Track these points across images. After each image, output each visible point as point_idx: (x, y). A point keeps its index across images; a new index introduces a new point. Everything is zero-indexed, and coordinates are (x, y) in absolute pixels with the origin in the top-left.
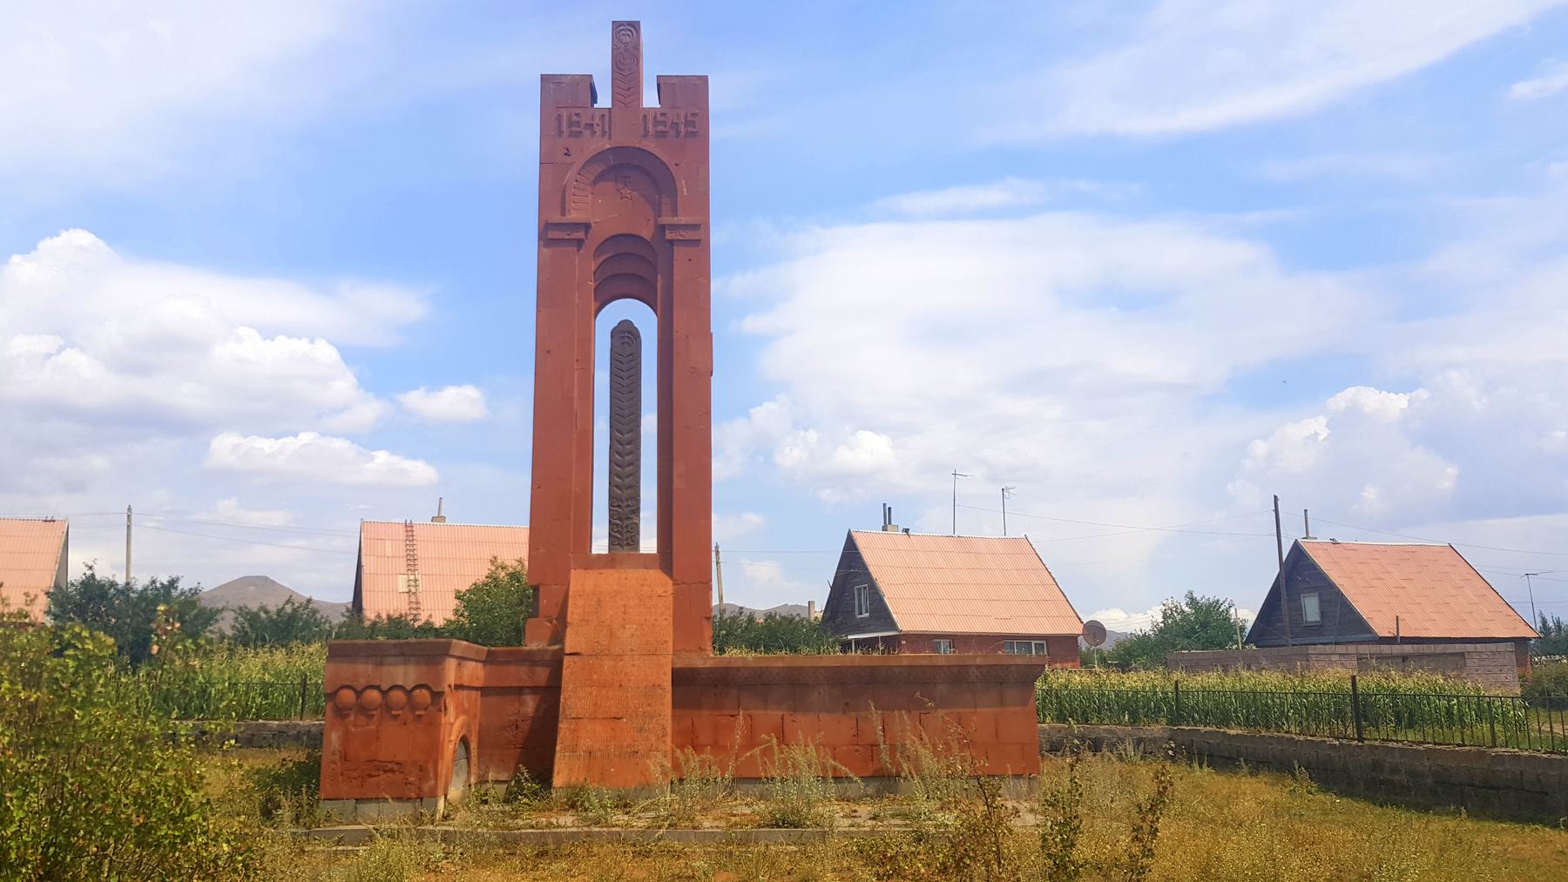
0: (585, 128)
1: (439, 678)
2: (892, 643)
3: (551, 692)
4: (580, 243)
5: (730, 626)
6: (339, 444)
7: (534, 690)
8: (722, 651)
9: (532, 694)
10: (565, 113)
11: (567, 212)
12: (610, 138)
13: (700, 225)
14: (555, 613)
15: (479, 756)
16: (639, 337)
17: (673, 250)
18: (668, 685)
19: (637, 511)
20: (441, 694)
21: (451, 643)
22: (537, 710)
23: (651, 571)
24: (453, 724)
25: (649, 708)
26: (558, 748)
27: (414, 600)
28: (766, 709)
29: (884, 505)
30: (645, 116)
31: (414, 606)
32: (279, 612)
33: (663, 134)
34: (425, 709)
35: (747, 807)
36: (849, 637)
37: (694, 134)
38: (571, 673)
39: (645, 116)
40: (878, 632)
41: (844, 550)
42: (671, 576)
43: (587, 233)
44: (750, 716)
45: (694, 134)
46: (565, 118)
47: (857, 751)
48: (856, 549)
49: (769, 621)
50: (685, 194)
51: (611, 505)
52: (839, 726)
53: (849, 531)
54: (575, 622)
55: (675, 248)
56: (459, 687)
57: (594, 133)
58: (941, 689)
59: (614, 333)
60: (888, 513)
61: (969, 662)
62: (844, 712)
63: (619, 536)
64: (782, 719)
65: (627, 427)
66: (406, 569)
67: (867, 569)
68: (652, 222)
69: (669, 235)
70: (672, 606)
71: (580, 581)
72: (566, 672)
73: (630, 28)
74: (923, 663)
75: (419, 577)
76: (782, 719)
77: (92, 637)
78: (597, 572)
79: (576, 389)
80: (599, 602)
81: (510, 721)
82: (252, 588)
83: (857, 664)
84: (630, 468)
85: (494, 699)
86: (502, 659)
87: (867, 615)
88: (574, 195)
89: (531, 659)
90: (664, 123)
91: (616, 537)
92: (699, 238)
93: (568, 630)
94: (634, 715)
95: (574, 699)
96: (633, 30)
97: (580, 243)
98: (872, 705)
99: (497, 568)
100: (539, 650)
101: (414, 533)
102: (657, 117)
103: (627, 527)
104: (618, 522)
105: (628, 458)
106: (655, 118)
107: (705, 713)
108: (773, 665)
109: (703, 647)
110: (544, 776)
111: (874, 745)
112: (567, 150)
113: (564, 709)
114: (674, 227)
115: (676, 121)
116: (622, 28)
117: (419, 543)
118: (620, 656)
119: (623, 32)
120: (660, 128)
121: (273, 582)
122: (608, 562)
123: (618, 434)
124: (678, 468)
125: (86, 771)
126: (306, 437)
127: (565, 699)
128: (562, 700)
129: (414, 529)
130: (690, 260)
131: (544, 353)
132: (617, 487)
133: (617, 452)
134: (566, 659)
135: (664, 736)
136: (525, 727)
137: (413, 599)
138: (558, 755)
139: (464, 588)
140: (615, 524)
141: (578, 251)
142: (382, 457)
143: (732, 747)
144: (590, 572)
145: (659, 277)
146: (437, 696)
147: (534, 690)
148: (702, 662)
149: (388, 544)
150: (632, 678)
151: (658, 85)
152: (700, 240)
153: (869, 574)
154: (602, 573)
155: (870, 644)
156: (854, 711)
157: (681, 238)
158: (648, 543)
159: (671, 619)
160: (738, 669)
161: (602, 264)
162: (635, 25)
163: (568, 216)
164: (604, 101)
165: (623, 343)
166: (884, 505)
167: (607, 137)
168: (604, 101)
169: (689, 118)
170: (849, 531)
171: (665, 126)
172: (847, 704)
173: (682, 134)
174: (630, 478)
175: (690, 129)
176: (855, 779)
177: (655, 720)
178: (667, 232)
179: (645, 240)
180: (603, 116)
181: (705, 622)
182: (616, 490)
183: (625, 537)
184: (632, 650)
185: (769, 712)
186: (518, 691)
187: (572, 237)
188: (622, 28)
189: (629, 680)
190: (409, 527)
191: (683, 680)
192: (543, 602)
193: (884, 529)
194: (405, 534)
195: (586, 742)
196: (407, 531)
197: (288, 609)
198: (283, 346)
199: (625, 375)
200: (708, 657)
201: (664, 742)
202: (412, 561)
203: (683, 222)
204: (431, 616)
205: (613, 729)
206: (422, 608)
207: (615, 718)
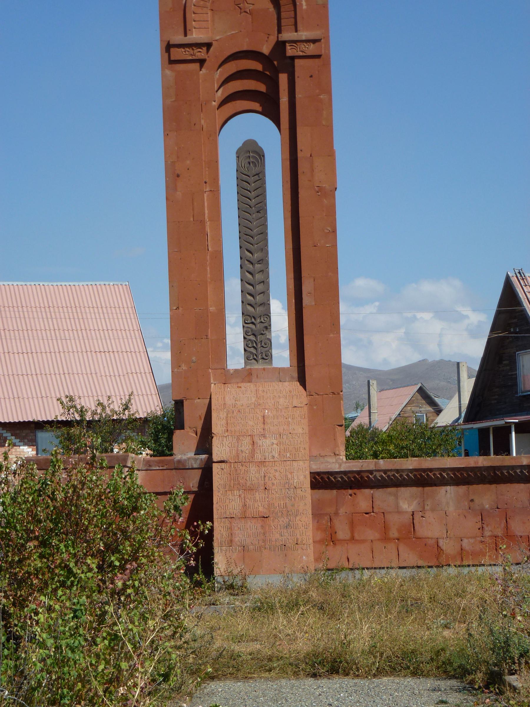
4: (202, 62)
13: (321, 39)
14: (199, 425)
16: (264, 156)
19: (268, 328)
23: (286, 384)
42: (305, 390)
59: (239, 153)
69: (290, 51)
70: (306, 416)
79: (206, 212)
86: (158, 468)
88: (194, 13)
91: (251, 353)
109: (337, 453)
124: (307, 287)
125: (106, 528)
130: (311, 76)
133: (248, 272)
134: (215, 466)
150: (275, 482)
154: (240, 387)
165: (249, 163)
207: (264, 517)
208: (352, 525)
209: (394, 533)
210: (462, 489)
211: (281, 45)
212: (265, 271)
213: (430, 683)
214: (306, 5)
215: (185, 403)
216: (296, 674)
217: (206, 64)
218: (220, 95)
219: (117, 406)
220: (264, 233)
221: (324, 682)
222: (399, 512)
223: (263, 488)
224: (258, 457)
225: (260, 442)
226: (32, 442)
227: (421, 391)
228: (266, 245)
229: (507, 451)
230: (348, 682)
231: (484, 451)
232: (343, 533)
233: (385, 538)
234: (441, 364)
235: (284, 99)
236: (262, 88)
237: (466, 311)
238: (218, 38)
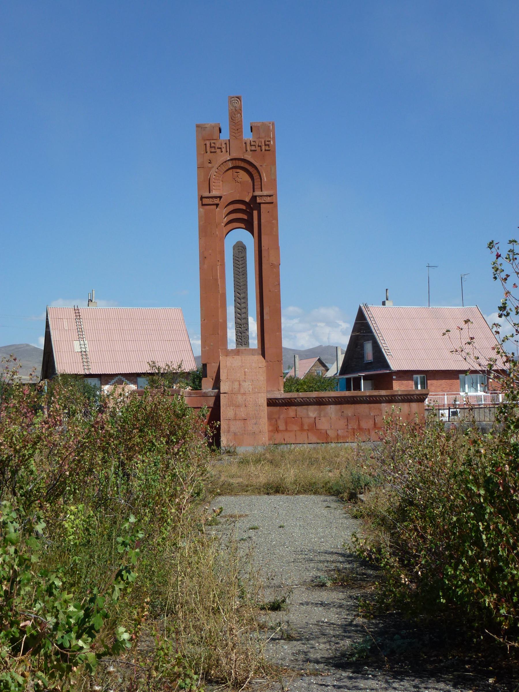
19: (247, 330)
30: (245, 143)
41: (356, 320)
46: (208, 145)
59: (234, 247)
63: (241, 341)
64: (315, 419)
67: (371, 332)
69: (259, 200)
73: (236, 99)
76: (315, 419)
96: (238, 100)
97: (217, 205)
101: (81, 317)
109: (280, 389)
110: (218, 444)
115: (260, 144)
116: (233, 99)
117: (84, 320)
119: (233, 101)
122: (237, 352)
129: (80, 311)
131: (203, 258)
148: (279, 395)
151: (251, 127)
157: (264, 202)
158: (254, 343)
168: (225, 136)
179: (245, 201)
189: (249, 404)
191: (272, 403)
194: (75, 315)
196: (79, 313)
208: (286, 423)
209: (306, 427)
210: (338, 407)
211: (254, 198)
212: (246, 303)
213: (322, 498)
214: (267, 179)
215: (207, 365)
216: (259, 493)
217: (219, 206)
218: (226, 220)
219: (175, 366)
220: (246, 285)
221: (272, 497)
222: (309, 417)
223: (244, 406)
224: (242, 391)
225: (243, 384)
226: (135, 383)
227: (319, 360)
229: (357, 387)
230: (284, 497)
231: (348, 389)
232: (282, 427)
233: (302, 429)
234: (329, 347)
235: (256, 223)
236: (245, 217)
237: (341, 323)
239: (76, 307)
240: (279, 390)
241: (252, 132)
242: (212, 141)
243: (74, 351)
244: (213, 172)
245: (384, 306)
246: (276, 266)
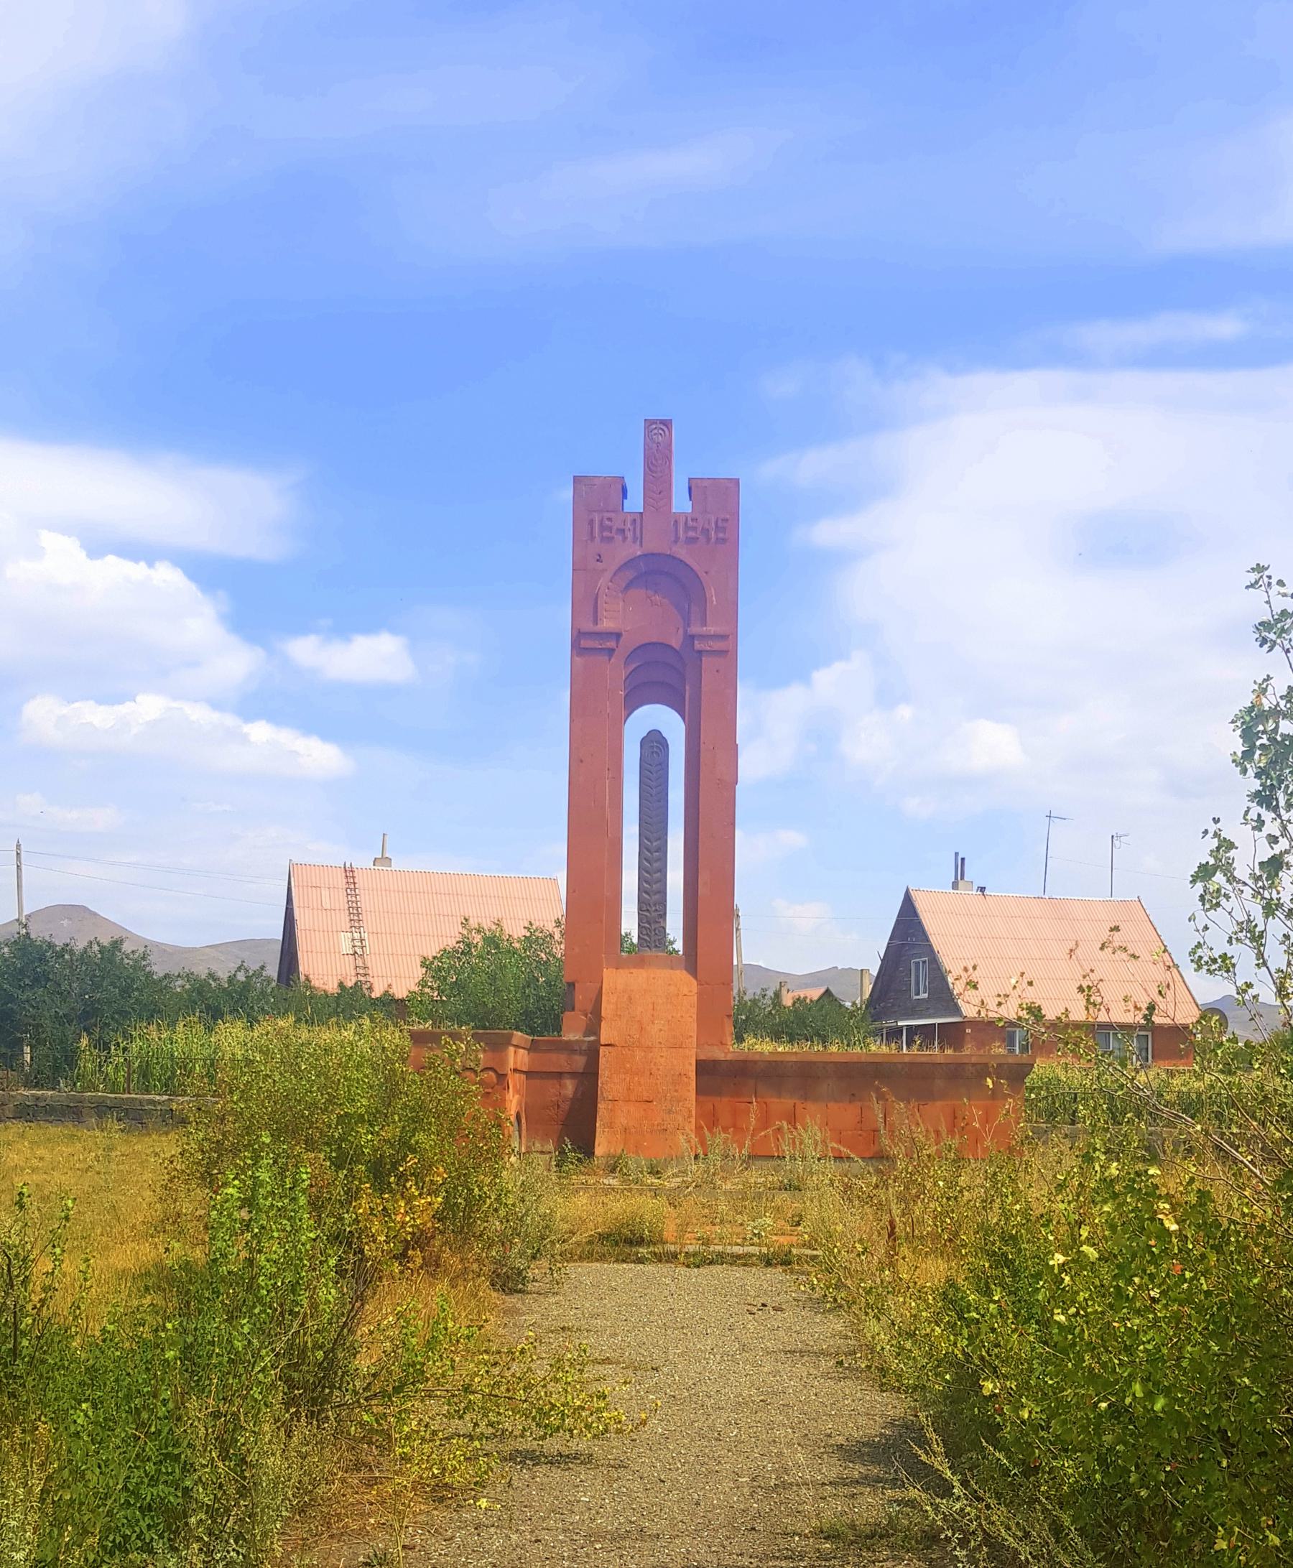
0: (617, 534)
1: (503, 1062)
2: (952, 1034)
3: (589, 1076)
5: (750, 1011)
6: (199, 714)
7: (573, 1074)
8: (740, 1039)
9: (571, 1078)
10: (597, 518)
11: (599, 622)
12: (641, 545)
14: (590, 1007)
15: (527, 1130)
17: (701, 660)
18: (693, 1075)
19: (663, 916)
20: (506, 1075)
21: (513, 1034)
22: (575, 1092)
23: (678, 972)
24: (513, 1102)
25: (676, 1094)
26: (598, 1125)
27: (361, 965)
28: (780, 1097)
29: (957, 854)
30: (676, 521)
31: (362, 971)
32: (231, 980)
33: (695, 540)
34: (492, 1088)
35: (757, 1176)
36: (900, 1024)
37: (724, 540)
38: (607, 1062)
39: (676, 521)
40: (933, 1017)
41: (898, 917)
42: (696, 977)
43: (618, 641)
44: (766, 1103)
45: (724, 540)
47: (860, 1135)
48: (915, 914)
49: (797, 1005)
50: (715, 603)
51: (640, 909)
52: (846, 1113)
53: (907, 891)
54: (609, 1016)
55: (703, 659)
56: (515, 1070)
57: (625, 539)
58: (939, 1083)
60: (960, 865)
61: (965, 1061)
62: (850, 1102)
64: (794, 1106)
65: (655, 835)
66: (349, 925)
67: (928, 940)
68: (681, 631)
69: (698, 645)
71: (614, 980)
72: (602, 1061)
74: (924, 1060)
75: (365, 936)
76: (794, 1106)
77: (454, 1044)
78: (627, 971)
79: (607, 802)
80: (630, 998)
81: (552, 1101)
82: (65, 922)
83: (863, 1060)
84: (659, 874)
85: (537, 1082)
87: (926, 995)
89: (569, 1048)
90: (695, 529)
91: (645, 940)
92: (725, 649)
93: (603, 1024)
94: (663, 1099)
95: (610, 1082)
96: (664, 428)
97: (611, 651)
98: (874, 1095)
99: (470, 931)
100: (577, 1041)
101: (357, 886)
102: (689, 522)
103: (655, 930)
104: (646, 925)
105: (656, 865)
106: (686, 523)
107: (725, 1099)
108: (787, 1060)
110: (586, 1147)
111: (876, 1131)
112: (600, 556)
113: (602, 1093)
114: (703, 637)
115: (706, 526)
116: (654, 426)
117: (362, 892)
118: (650, 1048)
119: (656, 431)
120: (691, 534)
121: (95, 914)
123: (647, 853)
124: (703, 877)
126: (149, 706)
127: (603, 1084)
128: (600, 1085)
129: (355, 874)
132: (646, 892)
133: (645, 859)
134: (602, 1049)
135: (689, 1117)
136: (566, 1106)
137: (360, 962)
138: (598, 1130)
139: (432, 950)
140: (644, 927)
141: (610, 660)
142: (260, 731)
143: (748, 1129)
144: (621, 971)
145: (687, 688)
146: (502, 1077)
147: (573, 1074)
148: (723, 1055)
149: (325, 893)
151: (690, 489)
152: (727, 652)
153: (931, 946)
155: (926, 1031)
156: (860, 1100)
157: (709, 649)
159: (695, 1016)
160: (755, 1062)
161: (630, 674)
162: (667, 423)
163: (599, 626)
164: (635, 502)
166: (957, 854)
167: (638, 543)
168: (635, 502)
169: (720, 524)
170: (907, 892)
171: (696, 533)
172: (853, 1095)
173: (713, 540)
174: (658, 885)
175: (721, 535)
176: (856, 1159)
177: (681, 1104)
178: (696, 642)
179: (675, 649)
180: (635, 520)
181: (726, 1020)
182: (644, 895)
183: (653, 939)
184: (660, 1043)
185: (782, 1100)
186: (559, 1075)
187: (604, 646)
188: (654, 426)
189: (659, 1069)
190: (349, 872)
191: (705, 1069)
192: (578, 997)
193: (955, 886)
194: (345, 881)
195: (622, 1120)
196: (353, 877)
197: (241, 977)
198: (115, 568)
199: (653, 784)
200: (729, 1052)
201: (690, 1122)
202: (355, 915)
203: (712, 633)
204: (390, 986)
205: (645, 1110)
206: (371, 975)
215: (576, 985)
228: (666, 834)
238: (628, 628)
239: (348, 865)
240: (722, 1043)
241: (690, 499)
242: (607, 515)
243: (339, 952)
244: (603, 582)
245: (955, 891)
246: (730, 914)
